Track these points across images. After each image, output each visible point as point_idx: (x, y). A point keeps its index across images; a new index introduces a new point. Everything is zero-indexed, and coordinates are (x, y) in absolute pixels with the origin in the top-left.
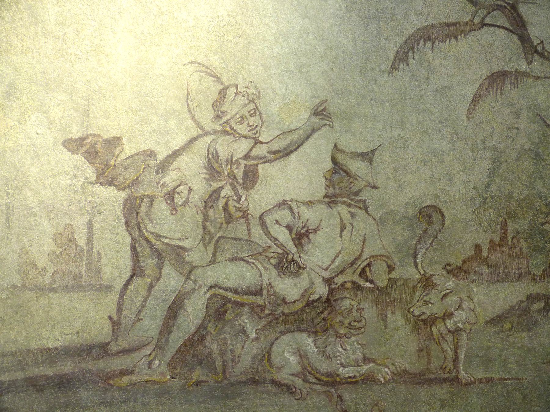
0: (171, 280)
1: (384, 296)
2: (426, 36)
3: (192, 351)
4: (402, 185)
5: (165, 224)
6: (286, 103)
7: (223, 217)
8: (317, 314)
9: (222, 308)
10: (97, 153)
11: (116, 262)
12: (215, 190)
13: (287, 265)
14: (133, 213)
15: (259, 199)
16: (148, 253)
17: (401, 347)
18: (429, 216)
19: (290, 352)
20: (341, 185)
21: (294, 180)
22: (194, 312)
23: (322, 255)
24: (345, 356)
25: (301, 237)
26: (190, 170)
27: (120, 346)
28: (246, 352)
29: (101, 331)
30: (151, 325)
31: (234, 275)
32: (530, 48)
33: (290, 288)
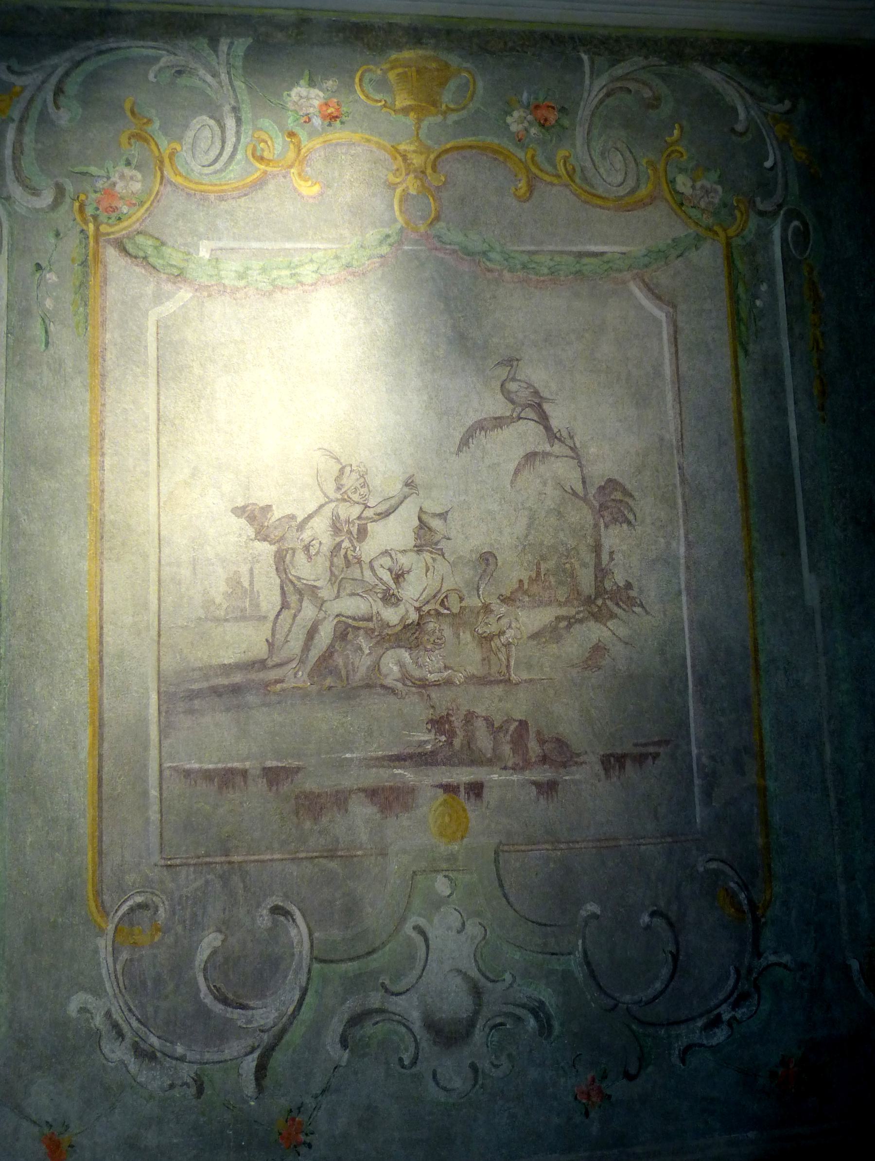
0: (309, 611)
1: (458, 619)
2: (481, 427)
3: (325, 665)
4: (467, 537)
5: (305, 570)
6: (386, 480)
7: (344, 563)
8: (411, 635)
10: (255, 516)
11: (269, 599)
12: (736, 317)
13: (389, 598)
14: (281, 561)
15: (369, 549)
16: (293, 591)
17: (471, 661)
18: (486, 559)
19: (394, 663)
20: (425, 537)
21: (392, 535)
23: (413, 590)
24: (431, 666)
25: (399, 577)
26: (320, 528)
28: (363, 663)
29: (260, 650)
30: (295, 645)
31: (353, 606)
32: (552, 435)
33: (392, 615)
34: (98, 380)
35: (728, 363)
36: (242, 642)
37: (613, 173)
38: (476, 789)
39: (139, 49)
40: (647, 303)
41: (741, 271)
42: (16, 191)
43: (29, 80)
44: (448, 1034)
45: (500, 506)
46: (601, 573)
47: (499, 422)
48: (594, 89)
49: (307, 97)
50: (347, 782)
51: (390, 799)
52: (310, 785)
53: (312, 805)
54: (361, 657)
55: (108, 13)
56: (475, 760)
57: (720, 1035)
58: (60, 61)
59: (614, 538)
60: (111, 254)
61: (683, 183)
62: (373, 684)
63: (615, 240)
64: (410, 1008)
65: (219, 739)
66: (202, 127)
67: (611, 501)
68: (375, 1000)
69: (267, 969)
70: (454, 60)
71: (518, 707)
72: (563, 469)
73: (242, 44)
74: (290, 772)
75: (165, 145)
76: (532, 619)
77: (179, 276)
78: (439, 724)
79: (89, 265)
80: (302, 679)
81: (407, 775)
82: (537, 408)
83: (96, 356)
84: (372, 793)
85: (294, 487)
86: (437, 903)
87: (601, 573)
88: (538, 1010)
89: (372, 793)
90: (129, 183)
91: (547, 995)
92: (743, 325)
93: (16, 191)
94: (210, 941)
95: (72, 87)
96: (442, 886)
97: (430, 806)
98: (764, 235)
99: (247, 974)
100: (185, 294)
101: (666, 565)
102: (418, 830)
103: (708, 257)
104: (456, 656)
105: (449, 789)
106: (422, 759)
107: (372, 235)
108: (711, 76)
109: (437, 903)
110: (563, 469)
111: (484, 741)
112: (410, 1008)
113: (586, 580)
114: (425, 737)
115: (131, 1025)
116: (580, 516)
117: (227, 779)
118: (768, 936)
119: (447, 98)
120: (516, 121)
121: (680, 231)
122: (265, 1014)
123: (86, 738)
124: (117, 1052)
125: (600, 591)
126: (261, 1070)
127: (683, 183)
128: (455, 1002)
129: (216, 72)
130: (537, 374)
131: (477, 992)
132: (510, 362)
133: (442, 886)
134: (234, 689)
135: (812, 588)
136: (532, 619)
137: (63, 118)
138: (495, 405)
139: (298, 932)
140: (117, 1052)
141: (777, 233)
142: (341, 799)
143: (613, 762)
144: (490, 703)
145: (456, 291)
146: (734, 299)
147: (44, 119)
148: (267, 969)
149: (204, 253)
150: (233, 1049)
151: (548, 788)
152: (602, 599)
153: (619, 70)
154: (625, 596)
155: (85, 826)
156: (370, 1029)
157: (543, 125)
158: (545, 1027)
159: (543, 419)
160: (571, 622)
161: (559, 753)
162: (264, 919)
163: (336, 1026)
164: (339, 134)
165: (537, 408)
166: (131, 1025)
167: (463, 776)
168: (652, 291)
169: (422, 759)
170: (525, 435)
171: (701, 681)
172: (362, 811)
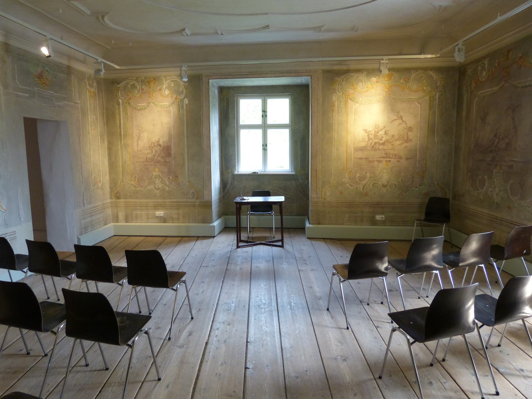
0: (371, 141)
1: (389, 142)
2: (394, 120)
3: (373, 147)
4: (391, 133)
5: (371, 136)
6: (381, 126)
7: (376, 136)
8: (383, 144)
9: (375, 143)
10: (365, 130)
11: (367, 140)
12: (430, 106)
13: (381, 140)
14: (368, 135)
15: (379, 134)
16: (369, 139)
17: (390, 147)
18: (393, 136)
19: (381, 147)
20: (386, 133)
21: (382, 133)
22: (373, 144)
23: (384, 139)
24: (385, 147)
25: (382, 137)
26: (373, 132)
27: (183, 90)
28: (377, 147)
29: (365, 145)
30: (369, 145)
31: (376, 141)
32: (403, 121)
33: (381, 142)
34: (347, 115)
35: (428, 112)
36: (363, 144)
37: (415, 87)
38: (390, 161)
39: (352, 74)
40: (418, 104)
41: (432, 99)
42: (338, 93)
43: (340, 79)
44: (384, 186)
45: (396, 129)
46: (408, 138)
47: (396, 120)
48: (413, 76)
49: (374, 79)
50: (375, 159)
51: (379, 162)
52: (370, 160)
53: (370, 162)
54: (377, 146)
55: (349, 70)
56: (390, 158)
57: (417, 189)
58: (343, 77)
59: (410, 133)
60: (349, 100)
61: (425, 88)
62: (378, 149)
63: (414, 96)
64: (380, 183)
65: (360, 154)
66: (361, 84)
67: (410, 129)
68: (376, 182)
69: (364, 178)
70: (394, 73)
71: (396, 152)
72: (404, 125)
73: (366, 73)
74: (368, 158)
75: (356, 86)
76: (398, 143)
77: (357, 103)
78: (386, 154)
79: (346, 101)
80: (370, 148)
81: (382, 159)
82: (401, 118)
83: (347, 112)
84: (377, 161)
85: (371, 128)
86: (384, 173)
87: (408, 138)
88: (395, 184)
89: (377, 161)
90: (351, 91)
91: (396, 183)
92: (431, 107)
93: (338, 93)
94: (358, 175)
95: (344, 80)
96: (385, 171)
97: (384, 163)
98: (436, 95)
99: (362, 178)
100: (358, 105)
101: (416, 138)
102: (382, 165)
103: (427, 98)
104: (388, 147)
105: (387, 161)
106: (383, 157)
107: (381, 97)
108: (431, 73)
109: (384, 173)
110: (404, 125)
111: (391, 156)
112: (380, 183)
113: (406, 139)
114: (384, 155)
115: (349, 182)
116: (406, 131)
117: (361, 159)
118: (424, 179)
119: (392, 78)
120: (402, 81)
121: (349, 100)
122: (364, 182)
123: (345, 154)
124: (348, 185)
125: (407, 140)
126: (363, 188)
127: (425, 88)
128: (385, 183)
129: (362, 76)
130: (402, 114)
131: (388, 182)
132: (398, 112)
133: (385, 171)
134: (362, 149)
135: (436, 140)
136: (398, 143)
137: (344, 84)
138: (396, 118)
139: (368, 175)
140: (348, 185)
141: (438, 94)
142: (374, 161)
143: (407, 159)
144: (392, 152)
145: (392, 103)
146: (430, 103)
147: (341, 84)
148: (364, 178)
149: (360, 99)
150: (360, 186)
151: (399, 161)
152: (408, 140)
153: (418, 72)
154: (411, 140)
155: (345, 163)
156: (375, 185)
157: (405, 81)
158: (396, 186)
159: (402, 119)
160: (403, 143)
161: (400, 158)
162: (364, 173)
163: (372, 184)
164: (378, 84)
165: (401, 118)
166: (349, 182)
167: (389, 159)
168: (419, 103)
169: (383, 157)
170: (400, 121)
171: (419, 150)
172: (376, 163)
